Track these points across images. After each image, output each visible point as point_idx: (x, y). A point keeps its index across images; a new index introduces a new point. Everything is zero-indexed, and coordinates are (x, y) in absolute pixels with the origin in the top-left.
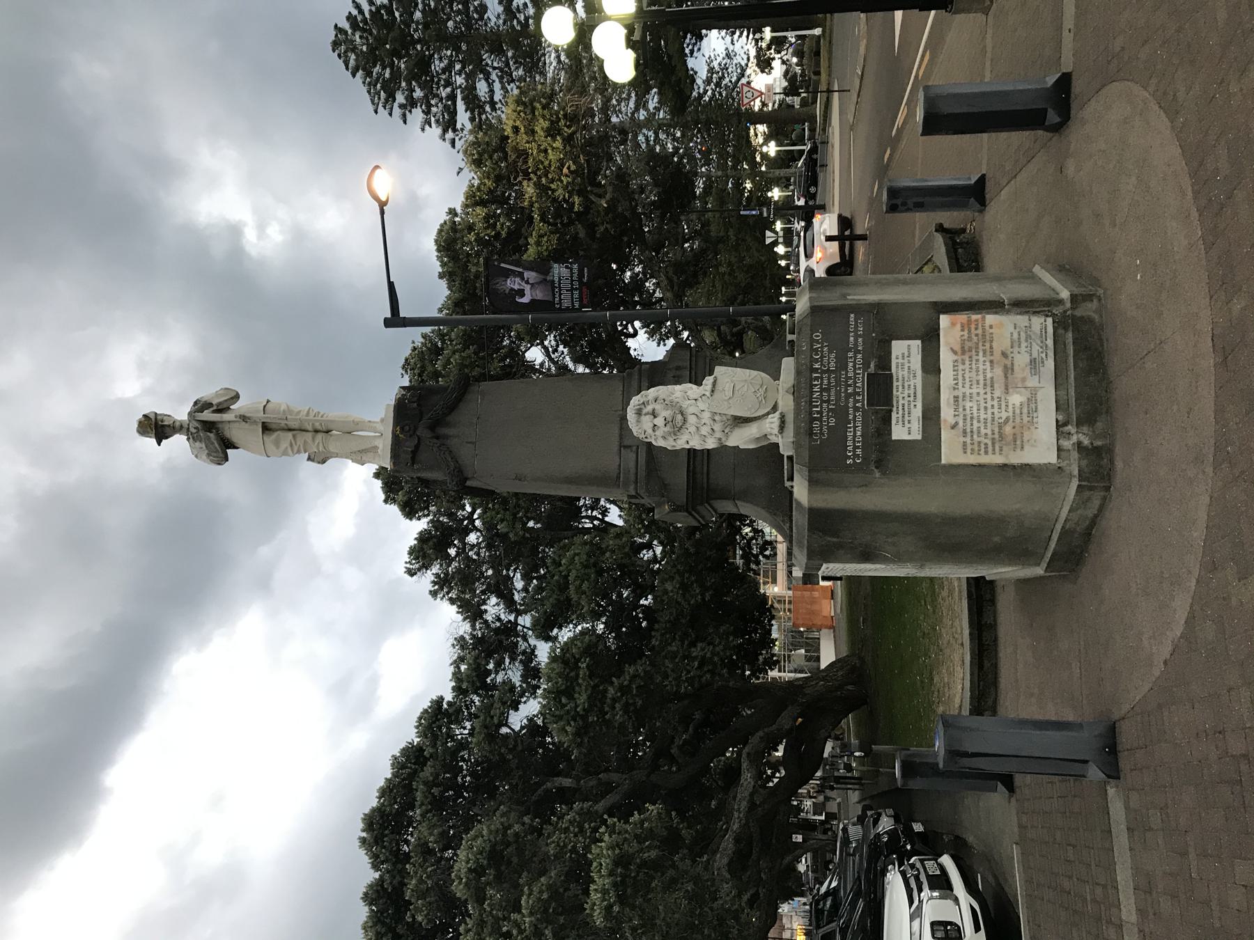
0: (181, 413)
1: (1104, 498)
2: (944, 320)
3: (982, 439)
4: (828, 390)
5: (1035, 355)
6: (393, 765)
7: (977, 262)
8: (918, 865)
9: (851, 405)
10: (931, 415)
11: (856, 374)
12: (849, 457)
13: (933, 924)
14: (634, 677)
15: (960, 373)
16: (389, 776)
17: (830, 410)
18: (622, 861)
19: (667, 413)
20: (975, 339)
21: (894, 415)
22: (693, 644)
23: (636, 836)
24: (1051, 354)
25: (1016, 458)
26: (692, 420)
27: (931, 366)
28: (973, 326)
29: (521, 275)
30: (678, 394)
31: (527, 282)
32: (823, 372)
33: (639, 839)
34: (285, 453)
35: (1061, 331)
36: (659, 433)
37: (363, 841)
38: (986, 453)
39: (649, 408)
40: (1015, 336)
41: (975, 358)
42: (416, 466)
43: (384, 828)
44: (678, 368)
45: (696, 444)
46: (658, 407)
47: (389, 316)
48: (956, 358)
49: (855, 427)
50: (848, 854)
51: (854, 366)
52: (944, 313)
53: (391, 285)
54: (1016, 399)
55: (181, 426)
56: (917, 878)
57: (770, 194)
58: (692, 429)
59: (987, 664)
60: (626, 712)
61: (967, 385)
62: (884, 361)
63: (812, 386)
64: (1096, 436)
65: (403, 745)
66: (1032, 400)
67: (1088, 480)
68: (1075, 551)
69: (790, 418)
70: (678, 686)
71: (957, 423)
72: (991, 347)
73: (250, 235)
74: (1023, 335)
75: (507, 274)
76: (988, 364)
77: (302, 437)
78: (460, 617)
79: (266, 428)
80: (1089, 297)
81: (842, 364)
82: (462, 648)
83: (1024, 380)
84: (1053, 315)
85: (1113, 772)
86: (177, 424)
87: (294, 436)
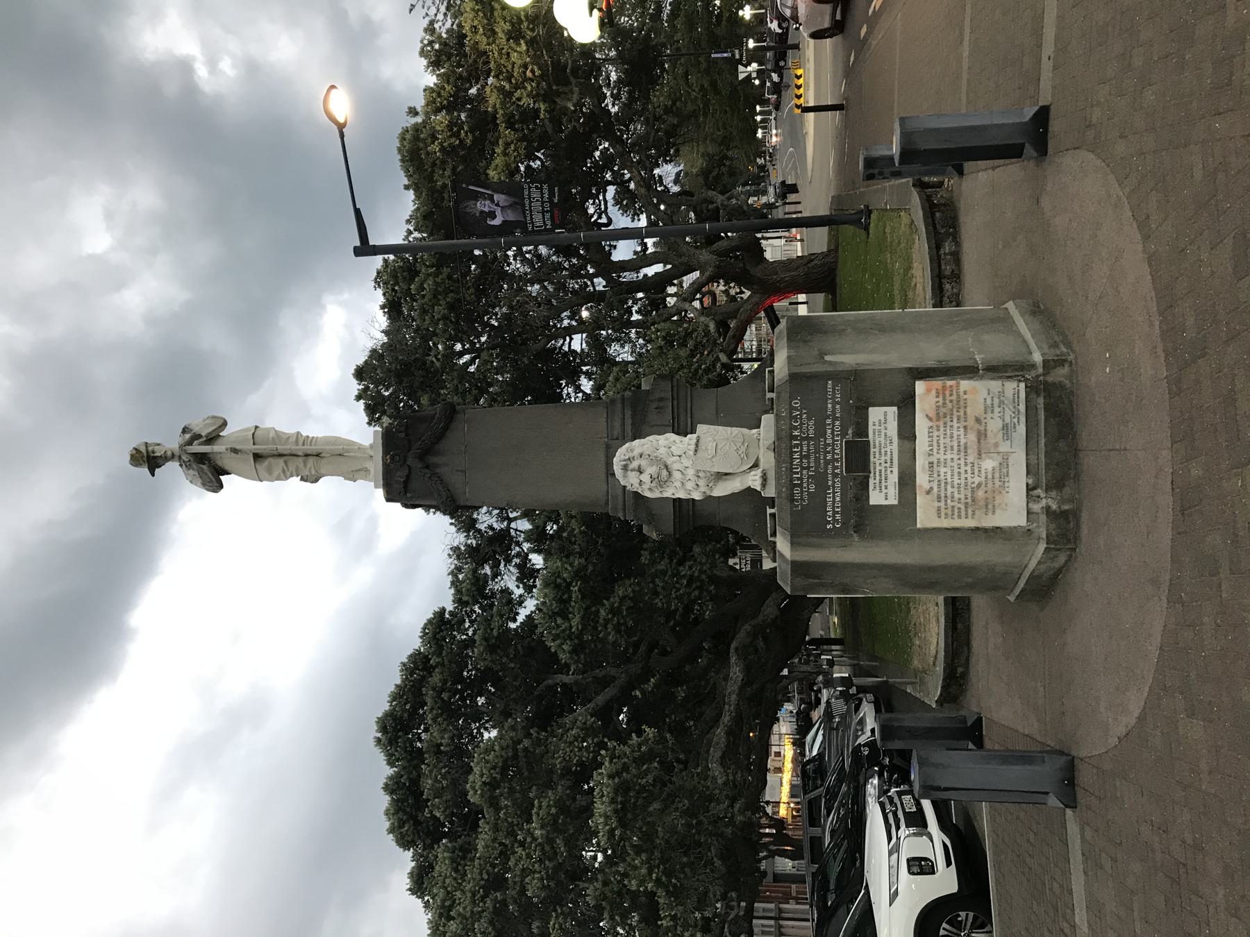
0: (171, 441)
1: (1070, 556)
2: (920, 387)
3: (955, 504)
4: (807, 457)
5: (1008, 420)
6: (402, 671)
7: (954, 227)
8: (896, 800)
9: (830, 471)
10: (907, 481)
11: (834, 441)
12: (829, 522)
13: (908, 860)
14: (623, 599)
15: (935, 439)
16: (399, 682)
17: (809, 477)
18: (622, 789)
19: (652, 470)
20: (949, 405)
21: (871, 482)
22: (681, 563)
23: (635, 760)
24: (1023, 419)
25: (989, 522)
26: (677, 475)
27: (907, 432)
28: (947, 393)
29: (491, 198)
30: (662, 451)
31: (497, 205)
32: (803, 439)
33: (639, 761)
34: (278, 479)
35: (1033, 396)
36: (645, 487)
37: (379, 741)
38: (959, 517)
39: (635, 464)
40: (989, 401)
41: (949, 424)
42: (409, 495)
43: (396, 730)
44: (661, 399)
45: (681, 495)
46: (643, 463)
47: (358, 244)
48: (931, 424)
49: (834, 493)
50: (832, 729)
51: (832, 433)
52: (920, 379)
53: (358, 213)
54: (989, 464)
55: (173, 456)
56: (895, 814)
57: (741, 13)
58: (678, 484)
59: (959, 626)
60: (618, 631)
61: (942, 451)
62: (862, 428)
63: (792, 453)
64: (1062, 501)
65: (411, 651)
66: (1004, 463)
67: (1055, 543)
68: (1044, 588)
69: (771, 475)
70: (669, 603)
71: (931, 488)
72: (965, 413)
73: (202, 71)
74: (996, 401)
75: (476, 196)
76: (962, 430)
77: (294, 463)
78: (453, 529)
79: (257, 457)
80: (1061, 362)
81: (820, 433)
82: (458, 558)
83: (996, 445)
84: (1026, 380)
85: (1071, 802)
86: (169, 453)
87: (286, 462)
